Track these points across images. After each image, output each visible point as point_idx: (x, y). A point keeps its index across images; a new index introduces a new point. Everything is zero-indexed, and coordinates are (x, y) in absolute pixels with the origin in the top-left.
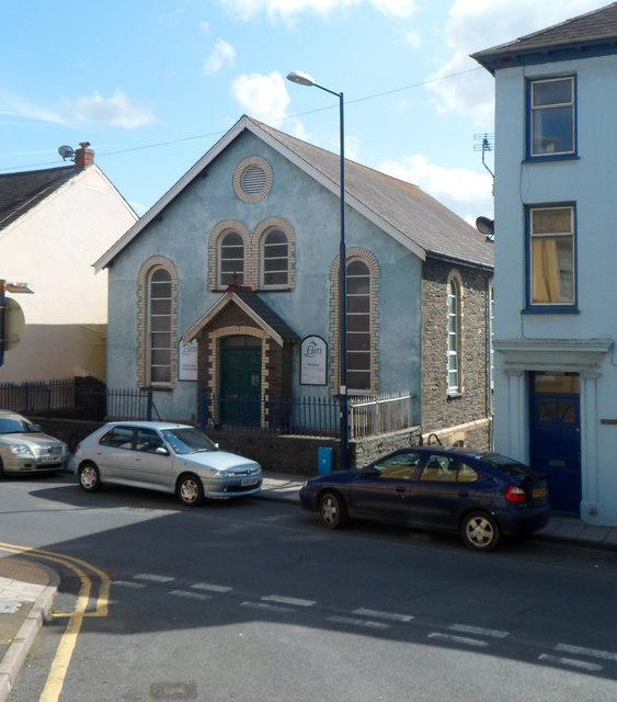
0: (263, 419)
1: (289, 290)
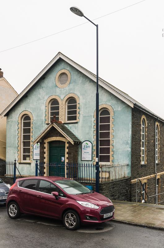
1: (77, 123)
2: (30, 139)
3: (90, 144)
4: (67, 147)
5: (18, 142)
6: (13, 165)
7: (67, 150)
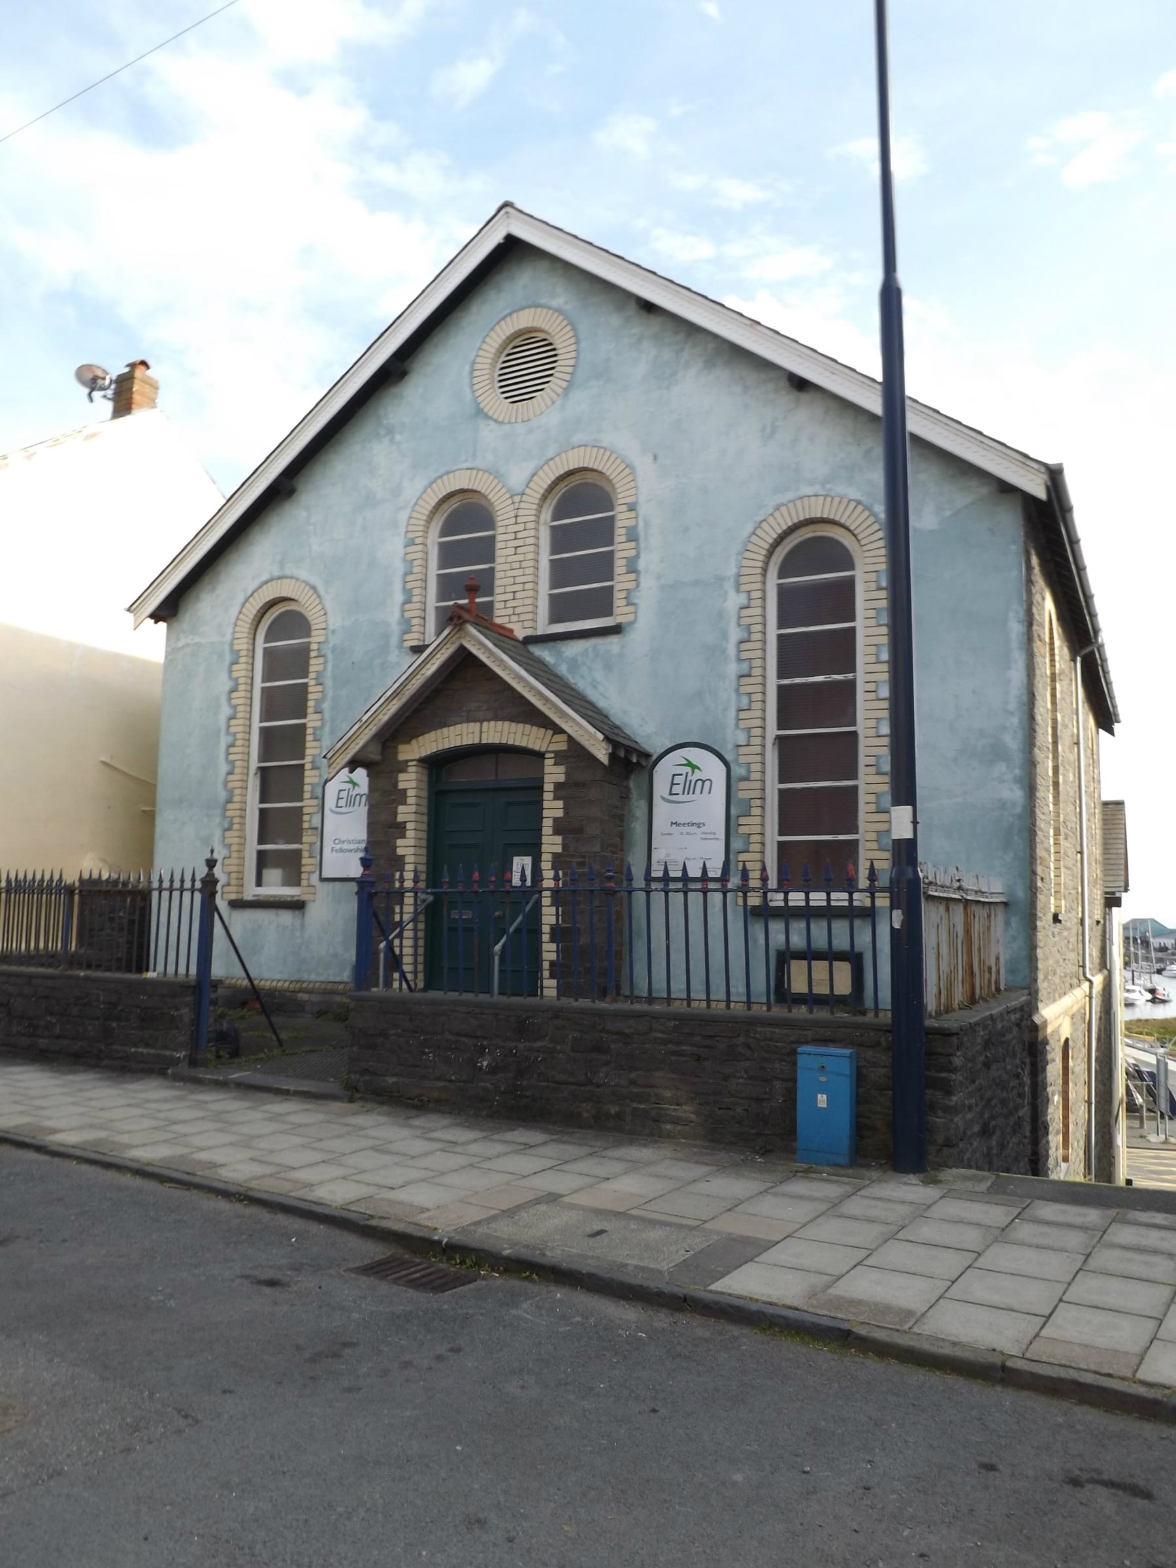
0: (546, 974)
1: (616, 630)
2: (303, 748)
3: (713, 769)
4: (558, 786)
5: (230, 773)
6: (198, 896)
7: (553, 809)
